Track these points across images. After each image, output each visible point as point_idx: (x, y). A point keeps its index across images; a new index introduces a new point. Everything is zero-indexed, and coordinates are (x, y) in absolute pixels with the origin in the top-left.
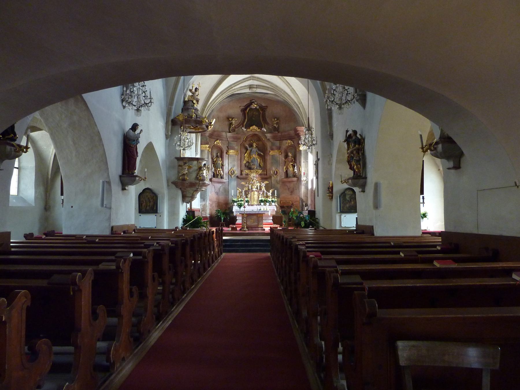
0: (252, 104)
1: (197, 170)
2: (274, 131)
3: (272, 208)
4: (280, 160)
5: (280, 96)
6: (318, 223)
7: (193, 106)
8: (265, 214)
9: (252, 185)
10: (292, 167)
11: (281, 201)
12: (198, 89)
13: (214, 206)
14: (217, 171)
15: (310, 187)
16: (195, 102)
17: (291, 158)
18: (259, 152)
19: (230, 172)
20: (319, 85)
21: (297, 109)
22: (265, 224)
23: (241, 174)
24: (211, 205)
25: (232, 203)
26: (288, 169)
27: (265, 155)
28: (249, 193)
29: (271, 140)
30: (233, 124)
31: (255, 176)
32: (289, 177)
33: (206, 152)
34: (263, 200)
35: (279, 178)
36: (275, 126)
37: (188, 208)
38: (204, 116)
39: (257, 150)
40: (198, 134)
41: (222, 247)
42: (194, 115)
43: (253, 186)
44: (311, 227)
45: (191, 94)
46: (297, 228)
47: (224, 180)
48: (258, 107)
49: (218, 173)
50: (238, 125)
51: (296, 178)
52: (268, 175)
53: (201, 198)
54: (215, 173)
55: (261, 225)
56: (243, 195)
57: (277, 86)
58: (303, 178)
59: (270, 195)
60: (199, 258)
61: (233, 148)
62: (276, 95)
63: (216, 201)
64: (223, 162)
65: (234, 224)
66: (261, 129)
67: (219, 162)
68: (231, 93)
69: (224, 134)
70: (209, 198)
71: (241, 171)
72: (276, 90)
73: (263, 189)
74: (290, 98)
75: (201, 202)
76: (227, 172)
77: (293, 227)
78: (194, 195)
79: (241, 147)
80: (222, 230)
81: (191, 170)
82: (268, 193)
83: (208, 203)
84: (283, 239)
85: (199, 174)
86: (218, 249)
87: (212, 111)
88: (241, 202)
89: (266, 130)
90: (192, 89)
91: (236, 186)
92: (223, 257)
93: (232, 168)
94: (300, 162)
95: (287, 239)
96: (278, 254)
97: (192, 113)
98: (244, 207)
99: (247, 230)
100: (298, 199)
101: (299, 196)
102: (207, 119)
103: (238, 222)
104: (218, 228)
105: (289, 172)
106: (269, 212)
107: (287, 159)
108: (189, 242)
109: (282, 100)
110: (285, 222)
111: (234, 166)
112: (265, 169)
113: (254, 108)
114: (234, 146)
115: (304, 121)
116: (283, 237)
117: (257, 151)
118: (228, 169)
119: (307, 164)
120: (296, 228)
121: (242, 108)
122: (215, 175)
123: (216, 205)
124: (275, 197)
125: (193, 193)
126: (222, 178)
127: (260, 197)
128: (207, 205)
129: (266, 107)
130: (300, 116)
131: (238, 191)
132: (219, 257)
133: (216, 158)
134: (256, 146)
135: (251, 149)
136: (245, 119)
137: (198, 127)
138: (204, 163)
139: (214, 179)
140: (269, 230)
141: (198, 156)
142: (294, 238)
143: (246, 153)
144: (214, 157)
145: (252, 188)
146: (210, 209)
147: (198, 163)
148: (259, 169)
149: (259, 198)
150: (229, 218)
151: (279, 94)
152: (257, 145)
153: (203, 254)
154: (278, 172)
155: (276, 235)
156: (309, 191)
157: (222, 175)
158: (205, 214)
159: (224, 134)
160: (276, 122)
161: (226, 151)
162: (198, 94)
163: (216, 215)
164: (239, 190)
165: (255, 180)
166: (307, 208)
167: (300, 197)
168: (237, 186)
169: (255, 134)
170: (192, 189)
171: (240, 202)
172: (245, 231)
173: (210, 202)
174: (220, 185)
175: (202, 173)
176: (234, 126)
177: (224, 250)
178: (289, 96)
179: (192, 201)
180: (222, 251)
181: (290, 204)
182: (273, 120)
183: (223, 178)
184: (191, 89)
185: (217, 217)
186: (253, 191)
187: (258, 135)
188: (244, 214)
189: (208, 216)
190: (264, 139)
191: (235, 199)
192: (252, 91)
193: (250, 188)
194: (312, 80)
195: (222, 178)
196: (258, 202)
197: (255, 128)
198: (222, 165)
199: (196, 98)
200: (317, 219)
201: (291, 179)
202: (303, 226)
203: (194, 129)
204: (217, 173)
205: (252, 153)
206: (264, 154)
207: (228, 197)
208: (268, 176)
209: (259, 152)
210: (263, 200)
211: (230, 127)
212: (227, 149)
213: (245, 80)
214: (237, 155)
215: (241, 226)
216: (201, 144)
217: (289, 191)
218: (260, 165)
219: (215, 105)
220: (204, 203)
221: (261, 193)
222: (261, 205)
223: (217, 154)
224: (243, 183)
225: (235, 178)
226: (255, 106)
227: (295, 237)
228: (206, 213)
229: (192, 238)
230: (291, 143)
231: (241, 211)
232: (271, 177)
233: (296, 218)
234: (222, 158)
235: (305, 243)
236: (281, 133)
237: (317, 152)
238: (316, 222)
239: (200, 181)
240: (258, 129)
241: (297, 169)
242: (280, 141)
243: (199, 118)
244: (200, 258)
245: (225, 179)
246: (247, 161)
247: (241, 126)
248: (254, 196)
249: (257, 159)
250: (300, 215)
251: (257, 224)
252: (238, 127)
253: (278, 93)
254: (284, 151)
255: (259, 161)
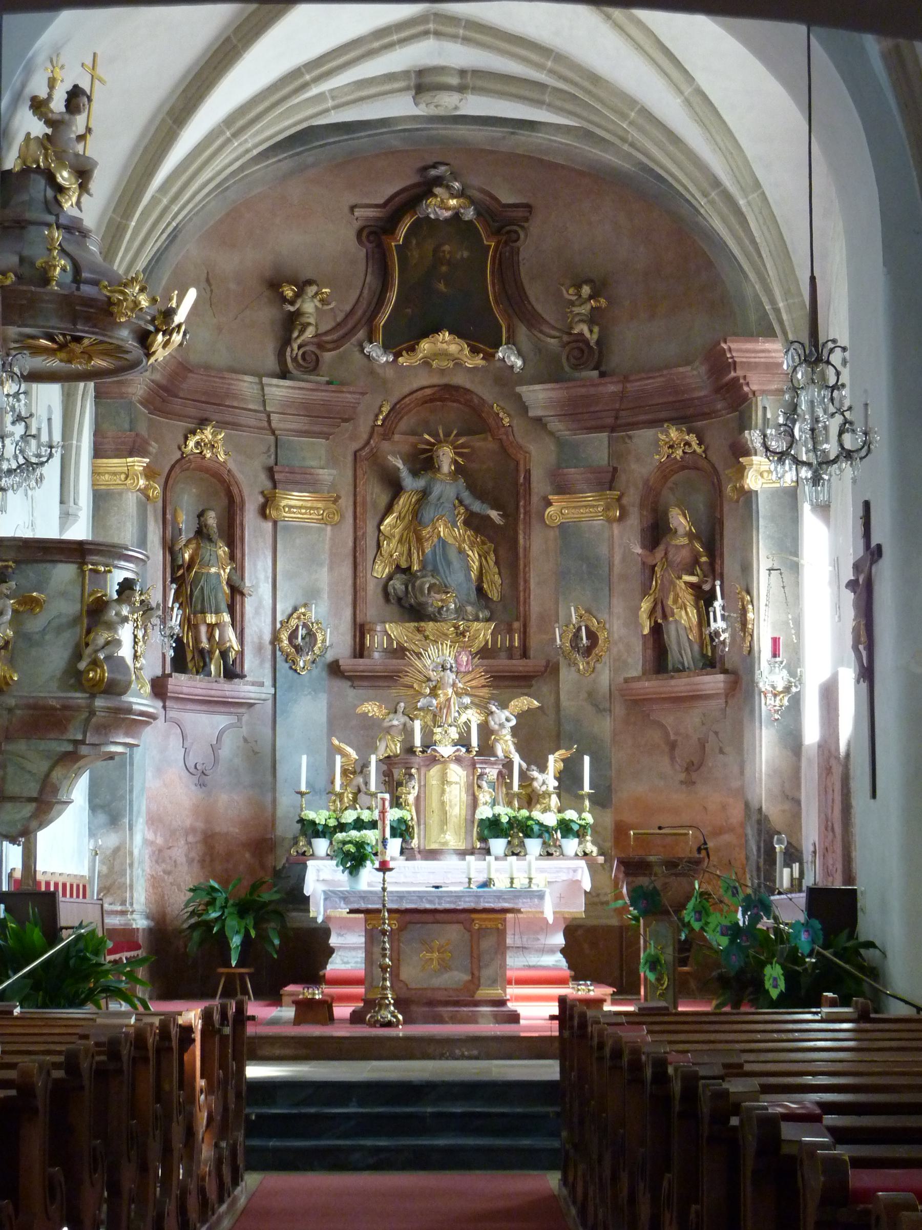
0: (429, 193)
1: (76, 621)
2: (575, 367)
3: (559, 870)
4: (617, 559)
5: (617, 142)
6: (874, 973)
7: (55, 208)
8: (518, 911)
9: (429, 718)
10: (697, 607)
11: (620, 830)
12: (89, 99)
13: (182, 859)
14: (203, 630)
15: (812, 734)
16: (64, 177)
17: (684, 541)
18: (477, 507)
19: (284, 636)
20: (878, 65)
21: (724, 220)
22: (521, 982)
23: (360, 651)
24: (160, 851)
25: (296, 842)
26: (665, 617)
27: (516, 519)
28: (411, 775)
29: (556, 425)
30: (305, 320)
31: (451, 660)
32: (678, 671)
33: (131, 501)
34: (505, 819)
35: (604, 678)
36: (581, 334)
37: (10, 876)
38: (119, 266)
39: (466, 495)
40: (82, 385)
41: (240, 1136)
42: (60, 267)
43: (437, 730)
44: (833, 1003)
45: (38, 128)
46: (736, 1005)
47: (242, 690)
48: (469, 214)
49: (205, 644)
50: (339, 325)
51: (721, 677)
52: (532, 653)
53: (95, 805)
54: (188, 639)
55: (493, 983)
56: (373, 788)
57: (595, 79)
58: (771, 672)
59: (551, 789)
60: (99, 1209)
61: (305, 481)
62: (588, 135)
63: (193, 830)
64: (239, 570)
65: (314, 977)
66: (489, 357)
67: (213, 570)
68: (294, 125)
69: (246, 385)
70: (144, 808)
71: (360, 630)
72: (580, 94)
73: (505, 745)
74: (680, 156)
75: (92, 834)
76: (267, 637)
77: (709, 1002)
78: (55, 790)
79: (359, 472)
80: (241, 1018)
81: (35, 625)
82: (535, 774)
83: (138, 839)
84: (661, 1077)
85: (89, 650)
86: (216, 1146)
87: (173, 238)
88: (364, 832)
89: (519, 363)
90: (50, 96)
91: (325, 730)
92: (249, 1200)
93: (295, 609)
94: (746, 569)
95: (691, 1080)
96: (624, 1177)
97: (50, 250)
98: (384, 867)
99: (400, 1017)
100: (736, 814)
101: (740, 792)
102: (142, 290)
103: (336, 965)
104: (216, 1002)
105: (671, 636)
106: (548, 898)
107: (660, 553)
108: (41, 1101)
109: (627, 166)
110: (654, 964)
111: (311, 595)
112: (517, 619)
113: (447, 221)
114: (313, 463)
115: (773, 302)
116: (660, 1064)
117: (461, 502)
118: (269, 619)
119: (797, 584)
120: (727, 1009)
121: (367, 219)
122: (189, 657)
123: (193, 854)
124: (582, 797)
125: (48, 775)
126: (232, 673)
127: (484, 796)
128: (136, 852)
129: (520, 213)
130: (746, 266)
131: (338, 758)
132: (221, 1201)
133: (193, 546)
134: (455, 462)
135: (421, 483)
136: (385, 287)
137: (86, 342)
138: (118, 576)
139: (180, 683)
140: (552, 1018)
141: (79, 531)
142: (735, 1070)
143: (388, 510)
144: (183, 539)
145: (428, 744)
146: (155, 882)
147: (82, 572)
148: (477, 619)
149: (474, 804)
150: (277, 942)
151: (611, 127)
152: (460, 460)
153: (128, 1178)
154: (602, 636)
155: (607, 1051)
156: (809, 761)
157: (232, 655)
158: (123, 913)
159: (246, 385)
160: (584, 309)
161: (261, 500)
162: (89, 130)
163: (193, 921)
164: (344, 755)
165: (450, 691)
166: (796, 874)
167: (747, 805)
168: (333, 727)
169: (447, 387)
170: (43, 745)
171: (354, 834)
172: (389, 1024)
173: (150, 836)
174: (221, 720)
175: (108, 643)
176: (310, 333)
177: (249, 1151)
178: (675, 139)
179: (42, 826)
180: (241, 1163)
181: (687, 849)
182: (570, 294)
183: (242, 676)
184: (43, 94)
185: (196, 935)
186: (434, 760)
187: (467, 391)
188: (378, 911)
189: (140, 923)
190: (506, 421)
191: (320, 816)
192: (432, 111)
193: (418, 742)
194: (833, 31)
195: (232, 673)
196: (469, 832)
197: (453, 348)
198: (236, 591)
199: (77, 155)
200: (870, 945)
201: (685, 681)
202: (774, 994)
203: (62, 355)
204: (197, 640)
205: (428, 513)
206: (511, 515)
207: (274, 801)
208: (535, 662)
209: (477, 507)
210: (505, 819)
211: (286, 341)
212: (268, 484)
213: (386, 40)
214: (335, 526)
215: (360, 990)
216: (98, 452)
217: (672, 759)
218: (480, 590)
219: (188, 202)
220: (110, 840)
221: (492, 773)
222: (488, 852)
223: (201, 515)
224: (372, 708)
225: (318, 672)
226: (453, 202)
227: (740, 1066)
228: (123, 903)
229: (58, 1074)
230: (687, 444)
231: (364, 896)
232: (558, 670)
233: (732, 941)
234: (231, 544)
235: (820, 1105)
236: (626, 379)
237: (867, 505)
238: (862, 968)
239: (93, 696)
240: (467, 351)
241: (723, 618)
242: (613, 429)
243: (95, 283)
244: (105, 1207)
245: (253, 684)
246: (398, 567)
247: (361, 334)
248: (443, 792)
249: (461, 551)
250: (755, 919)
251: (466, 977)
252: (338, 343)
253: (603, 123)
254: (638, 501)
255: (475, 566)
